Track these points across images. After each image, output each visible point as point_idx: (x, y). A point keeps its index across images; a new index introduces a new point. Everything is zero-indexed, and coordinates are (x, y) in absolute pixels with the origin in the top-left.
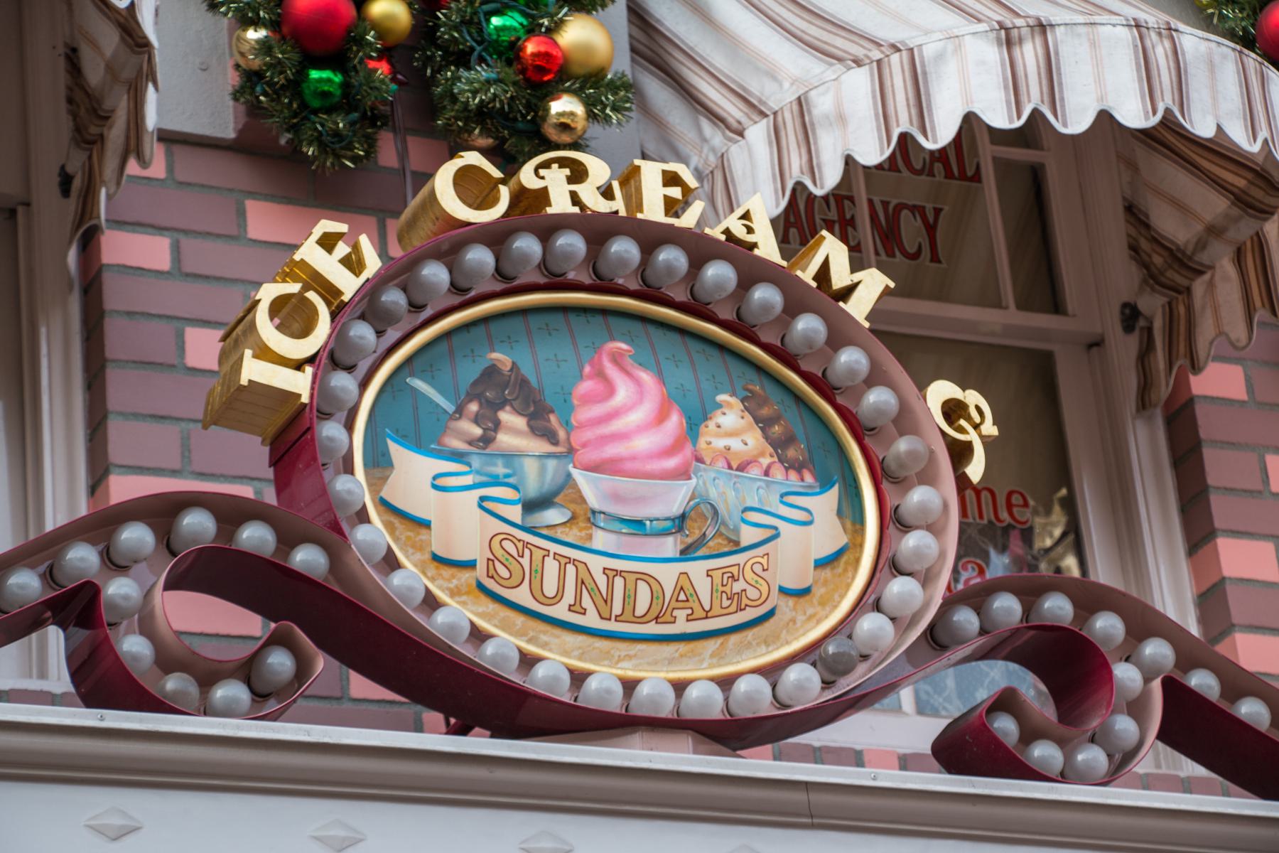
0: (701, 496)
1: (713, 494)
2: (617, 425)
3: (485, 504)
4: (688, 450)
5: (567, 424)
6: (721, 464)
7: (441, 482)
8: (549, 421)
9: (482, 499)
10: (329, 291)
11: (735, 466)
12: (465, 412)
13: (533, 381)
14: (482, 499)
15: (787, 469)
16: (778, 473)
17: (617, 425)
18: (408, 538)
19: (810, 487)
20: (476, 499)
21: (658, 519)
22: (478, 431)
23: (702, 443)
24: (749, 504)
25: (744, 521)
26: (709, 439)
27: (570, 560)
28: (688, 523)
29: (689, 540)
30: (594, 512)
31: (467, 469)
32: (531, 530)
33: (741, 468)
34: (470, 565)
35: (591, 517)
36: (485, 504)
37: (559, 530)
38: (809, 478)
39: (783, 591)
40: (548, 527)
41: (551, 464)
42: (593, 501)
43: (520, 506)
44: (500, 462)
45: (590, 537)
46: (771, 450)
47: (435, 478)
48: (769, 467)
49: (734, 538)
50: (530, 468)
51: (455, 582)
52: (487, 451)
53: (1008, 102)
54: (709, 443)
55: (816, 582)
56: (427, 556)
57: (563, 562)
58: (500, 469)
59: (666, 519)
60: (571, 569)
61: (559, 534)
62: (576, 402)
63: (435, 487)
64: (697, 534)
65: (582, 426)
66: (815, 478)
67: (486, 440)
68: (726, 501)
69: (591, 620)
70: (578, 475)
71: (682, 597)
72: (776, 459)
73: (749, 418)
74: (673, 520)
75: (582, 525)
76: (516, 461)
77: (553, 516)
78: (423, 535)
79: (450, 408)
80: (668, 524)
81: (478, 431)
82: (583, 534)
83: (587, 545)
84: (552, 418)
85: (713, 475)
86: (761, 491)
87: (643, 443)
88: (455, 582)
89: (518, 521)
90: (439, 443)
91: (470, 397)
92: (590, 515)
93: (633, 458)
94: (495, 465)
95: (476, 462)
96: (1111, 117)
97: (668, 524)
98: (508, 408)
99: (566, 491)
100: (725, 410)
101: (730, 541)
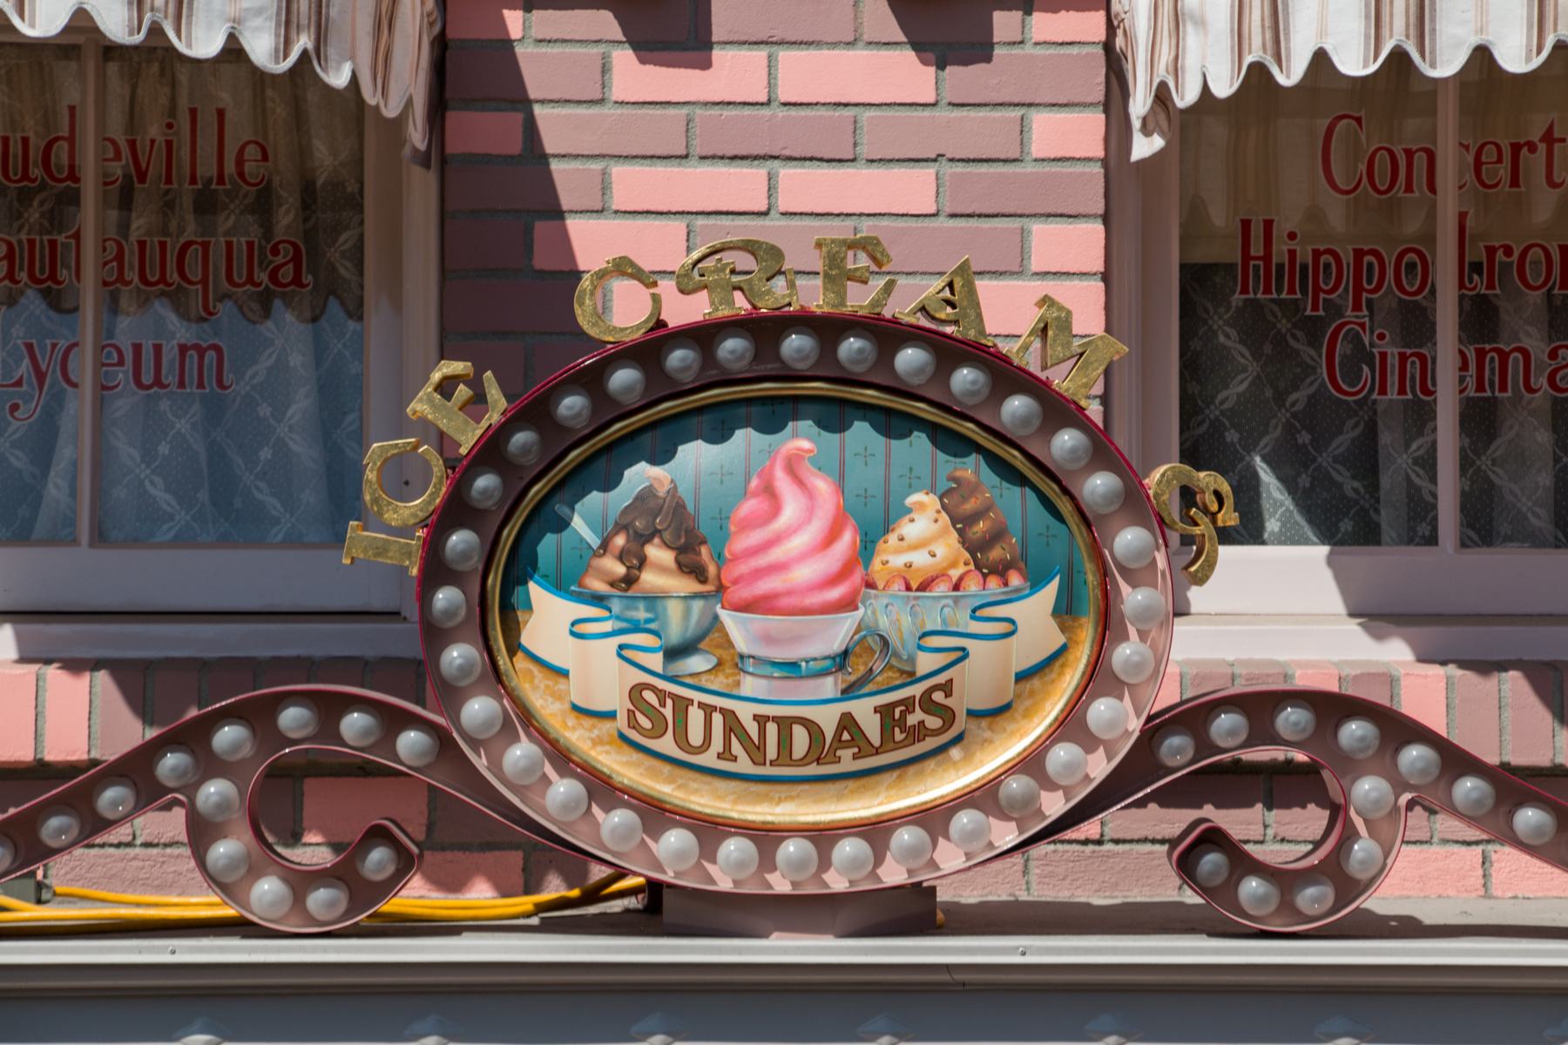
0: (868, 628)
1: (884, 623)
2: (776, 554)
3: (624, 653)
4: (857, 577)
5: (718, 557)
6: (898, 586)
7: (578, 629)
8: (699, 554)
9: (621, 647)
10: (443, 441)
11: (914, 585)
12: (610, 547)
13: (690, 507)
14: (621, 647)
15: (985, 576)
16: (972, 586)
17: (776, 554)
18: (547, 687)
19: (1017, 590)
20: (615, 647)
21: (815, 659)
22: (620, 570)
23: (876, 564)
24: (929, 627)
25: (920, 648)
26: (885, 558)
27: (715, 708)
28: (852, 659)
29: (852, 678)
30: (742, 657)
31: (607, 614)
32: (673, 679)
33: (923, 587)
34: (610, 716)
35: (739, 662)
36: (624, 653)
37: (704, 678)
38: (1015, 580)
39: (971, 714)
40: (691, 675)
41: (697, 605)
42: (741, 643)
43: (660, 655)
44: (641, 605)
45: (738, 684)
46: (967, 555)
47: (974, 611)
48: (961, 579)
49: (907, 668)
50: (674, 610)
51: (596, 732)
52: (629, 594)
53: (1367, 36)
54: (885, 563)
55: (1018, 696)
56: (567, 706)
57: (708, 710)
58: (641, 614)
59: (826, 658)
60: (717, 719)
61: (704, 682)
62: (733, 529)
63: (573, 634)
64: (862, 670)
65: (736, 558)
66: (1025, 579)
67: (629, 581)
68: (900, 630)
69: (744, 765)
70: (726, 616)
71: (846, 736)
72: (972, 567)
73: (945, 517)
74: (833, 658)
75: (728, 671)
76: (659, 603)
77: (697, 663)
78: (561, 685)
79: (594, 541)
80: (828, 663)
81: (620, 570)
82: (730, 680)
83: (735, 692)
84: (704, 550)
85: (885, 601)
86: (946, 610)
87: (805, 573)
88: (596, 732)
89: (659, 670)
90: (580, 585)
91: (620, 527)
92: (737, 660)
93: (789, 593)
94: (637, 609)
95: (616, 606)
96: (1491, 56)
97: (828, 663)
98: (656, 540)
99: (711, 636)
100: (913, 515)
101: (902, 672)
